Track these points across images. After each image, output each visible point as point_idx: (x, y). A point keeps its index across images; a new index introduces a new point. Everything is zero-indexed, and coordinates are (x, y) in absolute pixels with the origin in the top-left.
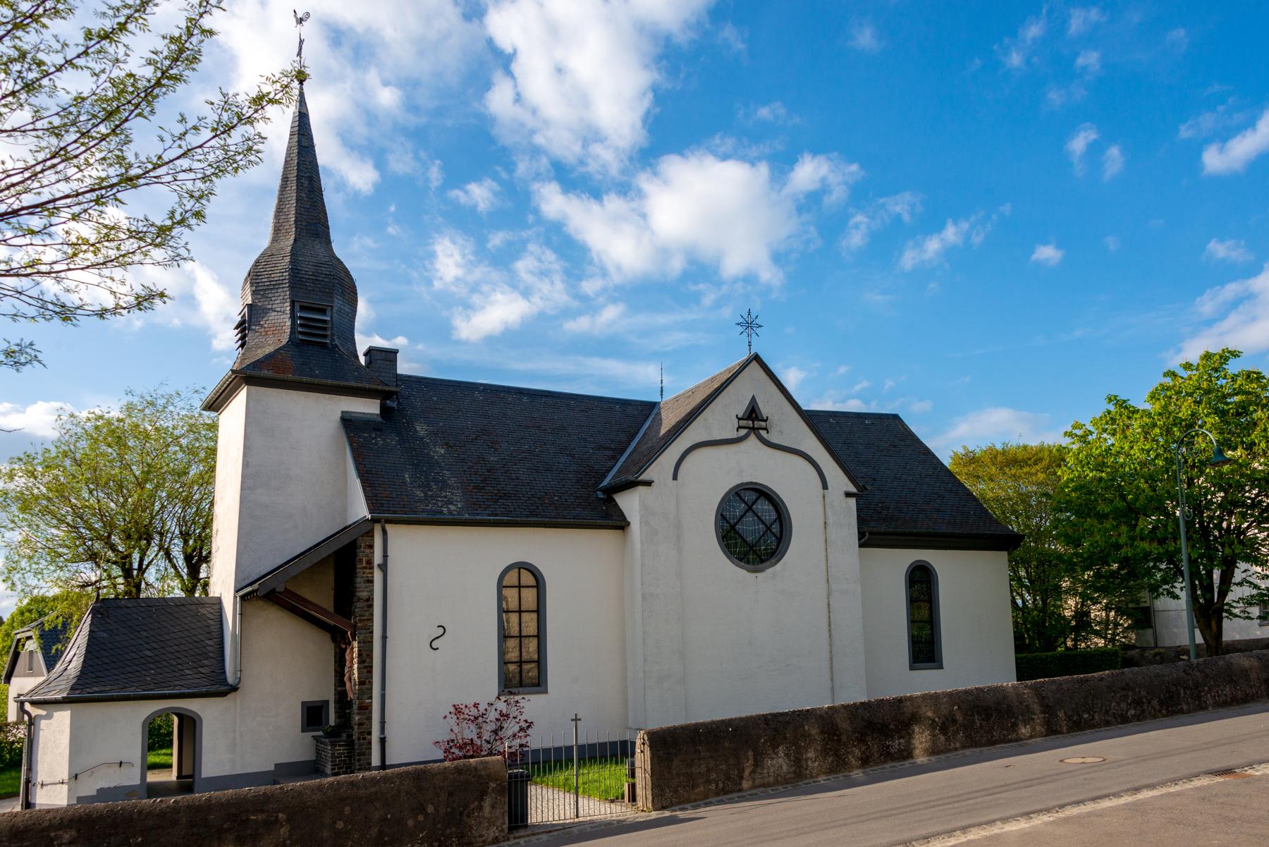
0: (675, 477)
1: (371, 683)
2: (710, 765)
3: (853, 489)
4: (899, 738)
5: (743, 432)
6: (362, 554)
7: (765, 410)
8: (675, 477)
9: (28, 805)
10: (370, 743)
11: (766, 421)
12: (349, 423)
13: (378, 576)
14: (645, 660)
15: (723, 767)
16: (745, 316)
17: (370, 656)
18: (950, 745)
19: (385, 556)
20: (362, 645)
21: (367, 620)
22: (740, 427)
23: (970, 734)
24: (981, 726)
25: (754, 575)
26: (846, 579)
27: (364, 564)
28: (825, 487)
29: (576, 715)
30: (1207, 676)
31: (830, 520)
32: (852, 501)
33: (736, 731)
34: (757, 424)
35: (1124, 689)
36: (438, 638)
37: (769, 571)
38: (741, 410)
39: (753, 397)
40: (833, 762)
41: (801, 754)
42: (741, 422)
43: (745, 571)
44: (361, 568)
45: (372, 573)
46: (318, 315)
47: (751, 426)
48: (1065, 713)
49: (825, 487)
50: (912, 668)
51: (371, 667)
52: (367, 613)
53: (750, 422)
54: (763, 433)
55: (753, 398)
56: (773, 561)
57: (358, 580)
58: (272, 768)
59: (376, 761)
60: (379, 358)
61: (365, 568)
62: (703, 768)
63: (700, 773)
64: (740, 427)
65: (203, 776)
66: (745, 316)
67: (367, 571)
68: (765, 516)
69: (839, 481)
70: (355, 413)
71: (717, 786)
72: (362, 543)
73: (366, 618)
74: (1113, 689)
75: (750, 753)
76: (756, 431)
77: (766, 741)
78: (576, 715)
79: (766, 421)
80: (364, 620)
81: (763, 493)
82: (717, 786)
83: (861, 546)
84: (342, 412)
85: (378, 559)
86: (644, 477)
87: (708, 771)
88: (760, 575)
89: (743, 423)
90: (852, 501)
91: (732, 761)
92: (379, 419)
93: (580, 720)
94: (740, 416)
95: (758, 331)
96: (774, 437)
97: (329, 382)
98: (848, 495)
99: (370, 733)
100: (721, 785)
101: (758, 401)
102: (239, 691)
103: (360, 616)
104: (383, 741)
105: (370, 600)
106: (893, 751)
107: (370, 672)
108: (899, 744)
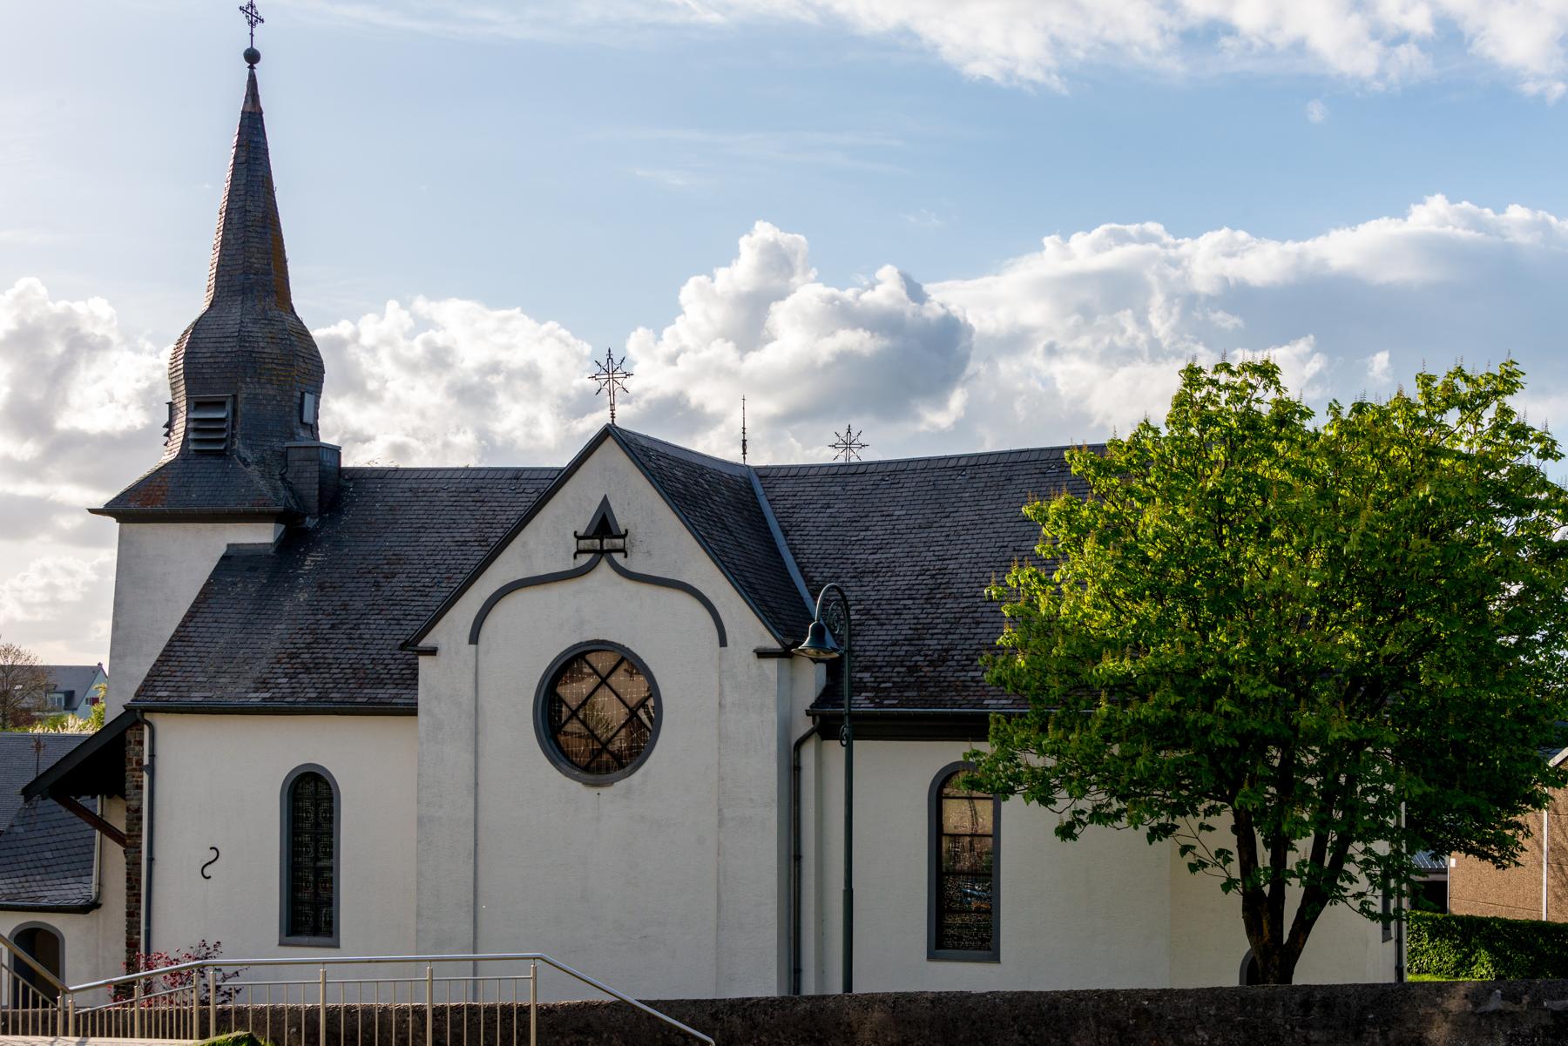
0: (474, 638)
1: (139, 914)
3: (772, 643)
5: (585, 559)
7: (622, 519)
8: (474, 638)
11: (623, 537)
14: (419, 915)
16: (604, 363)
17: (139, 881)
19: (152, 756)
20: (131, 867)
22: (579, 552)
25: (595, 790)
26: (751, 800)
27: (134, 766)
28: (723, 642)
30: (755, 1026)
31: (729, 698)
34: (607, 544)
35: (578, 1031)
36: (210, 863)
37: (623, 783)
38: (583, 523)
39: (605, 499)
42: (582, 542)
43: (579, 785)
45: (142, 777)
46: (211, 411)
47: (599, 548)
49: (723, 642)
50: (931, 956)
52: (137, 828)
53: (597, 541)
54: (618, 557)
55: (605, 502)
57: (127, 785)
60: (296, 458)
64: (579, 552)
66: (604, 363)
67: (137, 774)
68: (632, 693)
70: (242, 544)
72: (130, 735)
74: (560, 1030)
79: (623, 537)
84: (228, 545)
88: (604, 791)
89: (584, 544)
94: (581, 532)
96: (636, 564)
98: (762, 654)
101: (612, 504)
102: (102, 907)
107: (139, 901)
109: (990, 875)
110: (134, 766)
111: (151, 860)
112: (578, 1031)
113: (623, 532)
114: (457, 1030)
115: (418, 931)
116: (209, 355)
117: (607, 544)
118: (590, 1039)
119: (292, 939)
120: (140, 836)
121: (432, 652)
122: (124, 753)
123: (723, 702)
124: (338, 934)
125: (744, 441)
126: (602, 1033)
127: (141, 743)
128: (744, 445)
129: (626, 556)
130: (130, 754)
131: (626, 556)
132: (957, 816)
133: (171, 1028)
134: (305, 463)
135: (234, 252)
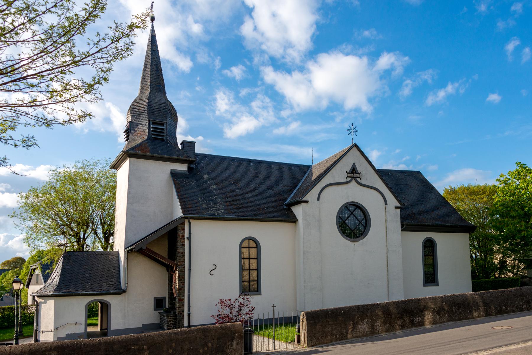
0: (318, 199)
1: (184, 289)
3: (399, 205)
4: (419, 317)
5: (349, 179)
6: (180, 233)
7: (359, 169)
8: (318, 199)
11: (359, 174)
12: (174, 174)
13: (187, 242)
14: (305, 281)
15: (339, 328)
17: (184, 278)
19: (190, 234)
20: (180, 273)
21: (183, 262)
22: (348, 177)
26: (395, 245)
27: (181, 237)
28: (386, 204)
29: (274, 305)
31: (388, 219)
34: (355, 175)
35: (521, 296)
38: (349, 169)
40: (388, 327)
42: (348, 174)
43: (349, 242)
45: (184, 241)
47: (353, 176)
48: (494, 306)
49: (386, 204)
50: (424, 286)
51: (184, 282)
52: (182, 259)
53: (353, 175)
54: (358, 179)
55: (354, 164)
56: (362, 237)
57: (178, 244)
58: (141, 326)
62: (330, 329)
63: (328, 331)
64: (348, 177)
67: (182, 240)
69: (393, 201)
70: (177, 170)
72: (180, 228)
73: (181, 261)
74: (517, 296)
75: (351, 323)
78: (274, 305)
79: (359, 174)
84: (171, 170)
85: (187, 235)
87: (333, 330)
88: (356, 243)
89: (349, 175)
90: (398, 211)
92: (187, 173)
93: (276, 307)
94: (348, 171)
95: (356, 133)
96: (363, 182)
98: (397, 207)
99: (183, 312)
101: (356, 165)
103: (179, 260)
104: (189, 315)
105: (183, 253)
106: (415, 322)
107: (184, 285)
108: (418, 319)
109: (425, 265)
111: (190, 270)
112: (521, 296)
115: (304, 286)
116: (157, 108)
117: (355, 175)
118: (524, 298)
119: (155, 300)
120: (184, 262)
122: (177, 233)
123: (387, 220)
126: (526, 296)
127: (184, 229)
129: (360, 179)
130: (179, 233)
131: (360, 179)
134: (190, 148)
135: (156, 78)
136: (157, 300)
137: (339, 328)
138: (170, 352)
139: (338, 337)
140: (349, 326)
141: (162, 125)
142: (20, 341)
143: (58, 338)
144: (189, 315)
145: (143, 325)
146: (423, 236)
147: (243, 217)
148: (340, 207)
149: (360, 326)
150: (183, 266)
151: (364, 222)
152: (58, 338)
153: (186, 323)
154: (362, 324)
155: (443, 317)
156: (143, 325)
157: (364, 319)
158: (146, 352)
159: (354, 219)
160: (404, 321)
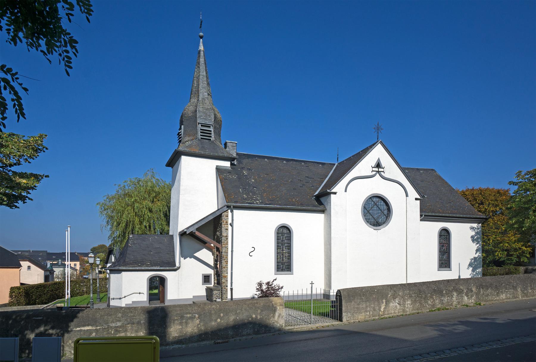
0: (346, 191)
1: (227, 268)
2: (367, 305)
3: (419, 197)
4: (448, 297)
5: (374, 173)
6: (224, 218)
7: (383, 164)
8: (346, 191)
9: (109, 305)
10: (227, 290)
11: (384, 168)
12: (219, 170)
13: (230, 228)
15: (373, 306)
18: (469, 301)
19: (233, 220)
21: (226, 244)
23: (478, 297)
24: (483, 294)
27: (225, 223)
28: (407, 196)
29: (312, 282)
32: (418, 202)
33: (378, 291)
34: (380, 170)
40: (419, 306)
41: (405, 302)
44: (224, 224)
45: (228, 226)
46: (208, 128)
47: (378, 170)
48: (521, 289)
49: (407, 196)
51: (227, 262)
54: (382, 173)
55: (379, 159)
56: (384, 225)
58: (192, 297)
59: (229, 297)
61: (225, 224)
62: (364, 306)
63: (363, 308)
64: (373, 171)
65: (168, 299)
67: (226, 225)
69: (413, 194)
71: (370, 313)
73: (225, 243)
75: (384, 301)
76: (379, 172)
77: (391, 296)
78: (312, 282)
79: (384, 168)
80: (225, 244)
81: (381, 198)
82: (370, 313)
83: (421, 220)
85: (230, 221)
86: (333, 191)
87: (367, 307)
89: (374, 169)
90: (418, 202)
91: (376, 303)
92: (230, 169)
93: (314, 284)
94: (373, 166)
95: (382, 131)
96: (386, 175)
97: (430, 214)
98: (416, 199)
99: (227, 286)
100: (371, 313)
103: (223, 242)
104: (232, 289)
105: (227, 237)
106: (444, 302)
108: (447, 299)
110: (225, 223)
111: (232, 251)
113: (383, 167)
114: (340, 297)
119: (204, 277)
121: (335, 193)
124: (293, 270)
125: (338, 158)
128: (338, 159)
132: (278, 235)
133: (335, 316)
136: (204, 276)
137: (373, 306)
138: (219, 321)
139: (371, 313)
140: (382, 304)
141: (201, 138)
142: (381, 310)
143: (126, 304)
144: (232, 289)
145: (193, 296)
146: (110, 300)
147: (162, 268)
148: (365, 199)
149: (392, 304)
150: (227, 247)
151: (386, 212)
152: (126, 304)
153: (229, 297)
154: (394, 302)
155: (471, 298)
156: (193, 296)
157: (396, 298)
158: (198, 320)
159: (377, 209)
160: (433, 301)
